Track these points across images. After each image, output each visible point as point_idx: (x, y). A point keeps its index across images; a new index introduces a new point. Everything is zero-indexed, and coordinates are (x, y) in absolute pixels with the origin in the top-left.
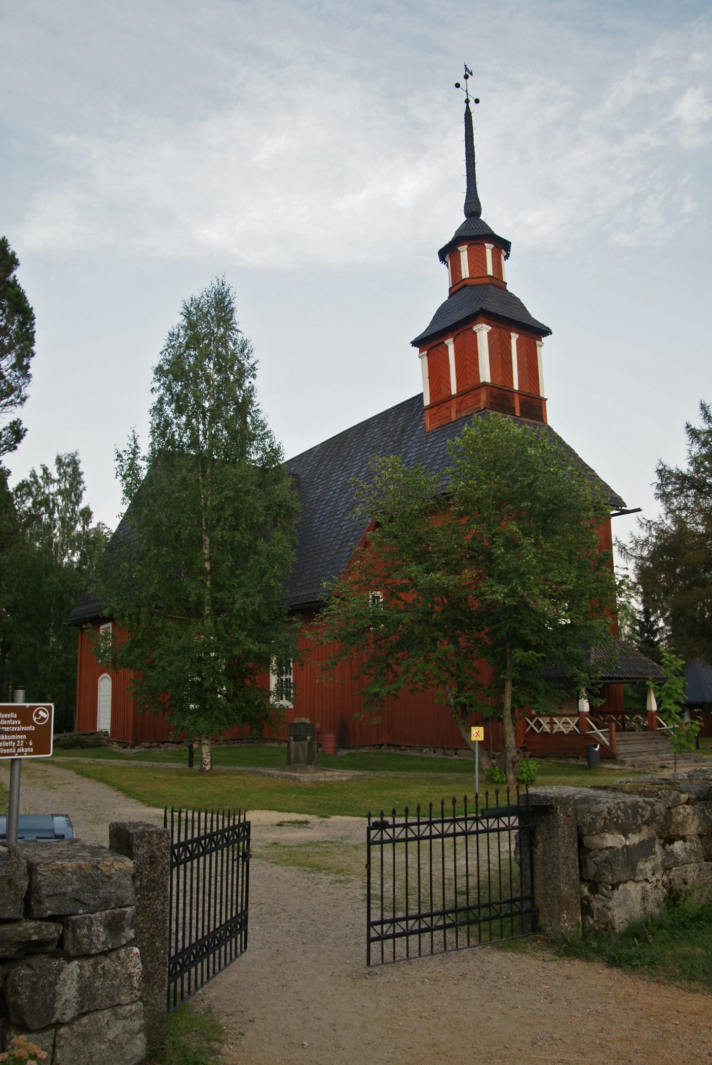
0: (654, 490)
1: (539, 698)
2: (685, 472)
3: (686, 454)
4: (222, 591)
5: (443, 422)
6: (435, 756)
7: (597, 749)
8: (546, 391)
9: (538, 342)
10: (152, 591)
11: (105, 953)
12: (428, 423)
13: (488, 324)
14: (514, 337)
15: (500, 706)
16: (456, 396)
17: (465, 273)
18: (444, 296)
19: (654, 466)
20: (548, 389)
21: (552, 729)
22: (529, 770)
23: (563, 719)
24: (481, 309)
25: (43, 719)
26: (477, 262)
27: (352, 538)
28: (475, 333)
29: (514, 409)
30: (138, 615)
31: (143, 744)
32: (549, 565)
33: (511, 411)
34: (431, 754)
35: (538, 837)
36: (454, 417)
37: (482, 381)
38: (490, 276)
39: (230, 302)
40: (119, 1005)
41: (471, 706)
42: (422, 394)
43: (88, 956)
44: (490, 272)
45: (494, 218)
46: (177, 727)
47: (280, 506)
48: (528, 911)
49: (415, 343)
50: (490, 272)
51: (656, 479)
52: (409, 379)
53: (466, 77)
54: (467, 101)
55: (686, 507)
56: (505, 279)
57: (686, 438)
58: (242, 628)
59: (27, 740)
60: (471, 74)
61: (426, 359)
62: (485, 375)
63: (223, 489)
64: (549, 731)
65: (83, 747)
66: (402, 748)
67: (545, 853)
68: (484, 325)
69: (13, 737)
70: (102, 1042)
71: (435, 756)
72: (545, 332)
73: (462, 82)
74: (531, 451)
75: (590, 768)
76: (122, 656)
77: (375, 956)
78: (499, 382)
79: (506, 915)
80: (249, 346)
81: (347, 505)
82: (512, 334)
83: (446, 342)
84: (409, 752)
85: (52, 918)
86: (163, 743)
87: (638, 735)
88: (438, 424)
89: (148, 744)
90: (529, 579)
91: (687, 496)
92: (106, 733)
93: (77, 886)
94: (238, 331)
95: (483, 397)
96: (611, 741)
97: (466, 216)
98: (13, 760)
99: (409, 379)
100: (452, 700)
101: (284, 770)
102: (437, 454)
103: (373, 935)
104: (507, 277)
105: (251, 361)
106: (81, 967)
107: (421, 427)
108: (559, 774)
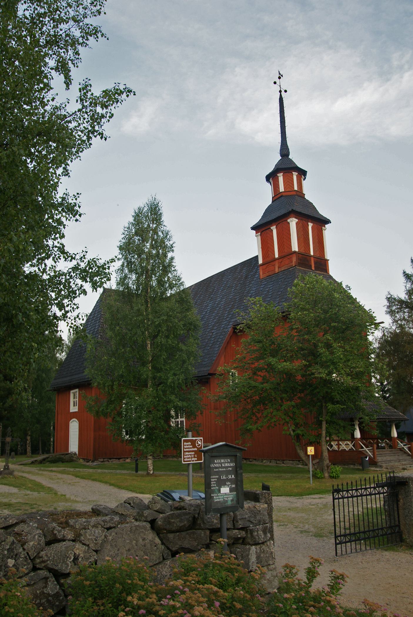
0: (385, 309)
1: (340, 431)
2: (403, 298)
3: (404, 289)
4: (160, 372)
5: (270, 273)
6: (271, 464)
7: (367, 459)
8: (328, 255)
9: (323, 228)
10: (121, 373)
11: (263, 543)
12: (261, 273)
13: (296, 218)
14: (310, 225)
15: (319, 436)
16: (278, 259)
17: (282, 189)
18: (270, 202)
19: (385, 295)
20: (329, 254)
21: (339, 448)
22: (336, 471)
23: (346, 442)
24: (292, 210)
25: (199, 445)
26: (288, 182)
27: (220, 340)
28: (289, 223)
29: (311, 266)
30: (112, 386)
31: (99, 460)
32: (349, 357)
33: (310, 267)
34: (268, 463)
35: (400, 497)
36: (277, 270)
37: (293, 250)
38: (296, 191)
39: (159, 210)
40: (269, 565)
41: (303, 435)
42: (257, 256)
43: (259, 544)
44: (296, 188)
45: (296, 158)
46: (136, 450)
47: (191, 324)
48: (398, 532)
49: (253, 228)
50: (296, 188)
51: (386, 303)
52: (250, 248)
53: (279, 78)
54: (280, 91)
55: (404, 319)
56: (304, 192)
57: (403, 279)
58: (172, 393)
59: (194, 455)
60: (282, 76)
61: (259, 237)
62: (295, 247)
63: (161, 315)
64: (337, 449)
65: (63, 462)
66: (251, 460)
67: (404, 504)
68: (294, 219)
69: (190, 453)
70: (265, 580)
71: (271, 464)
72: (327, 221)
73: (278, 81)
74: (336, 295)
75: (363, 470)
76: (103, 410)
77: (339, 551)
78: (302, 251)
79: (389, 534)
80: (169, 233)
81: (215, 320)
82: (309, 224)
83: (272, 228)
84: (254, 462)
85: (242, 529)
86: (110, 459)
87: (387, 451)
88: (267, 274)
89: (102, 460)
90: (339, 365)
91: (404, 312)
92: (75, 454)
93: (249, 515)
94: (164, 226)
95: (294, 259)
96: (374, 455)
97: (281, 156)
98: (189, 464)
99: (250, 248)
100: (292, 432)
101: (198, 473)
102: (268, 292)
103: (338, 542)
104: (305, 191)
105: (171, 242)
106: (256, 548)
107: (257, 276)
108: (347, 474)
